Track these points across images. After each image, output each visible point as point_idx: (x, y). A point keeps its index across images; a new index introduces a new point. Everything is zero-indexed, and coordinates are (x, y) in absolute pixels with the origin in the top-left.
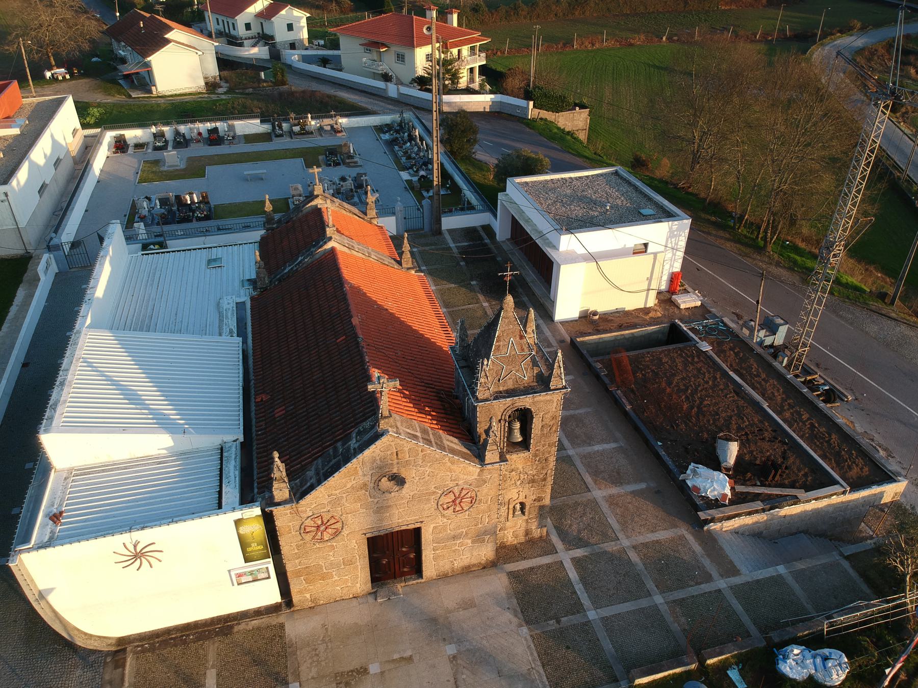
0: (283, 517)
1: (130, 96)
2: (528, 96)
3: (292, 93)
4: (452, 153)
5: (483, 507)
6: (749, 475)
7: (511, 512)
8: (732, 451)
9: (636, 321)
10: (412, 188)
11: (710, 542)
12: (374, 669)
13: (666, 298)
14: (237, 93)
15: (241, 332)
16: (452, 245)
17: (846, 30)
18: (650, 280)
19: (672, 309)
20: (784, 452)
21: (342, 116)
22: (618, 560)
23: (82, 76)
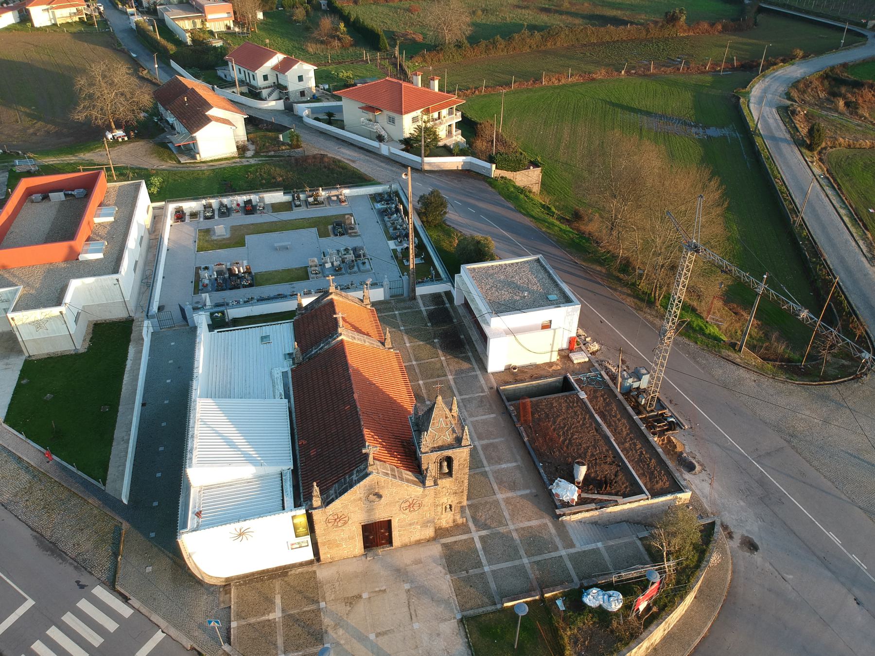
0: (317, 515)
1: (179, 162)
2: (491, 160)
3: (305, 158)
4: (426, 224)
5: (426, 508)
6: (591, 487)
8: (582, 472)
9: (543, 373)
10: (396, 257)
11: (561, 528)
12: (365, 596)
13: (565, 356)
14: (262, 156)
15: (287, 396)
16: (423, 309)
17: (788, 58)
18: (552, 345)
19: (569, 364)
20: (617, 472)
21: (345, 187)
22: (506, 538)
23: (139, 136)
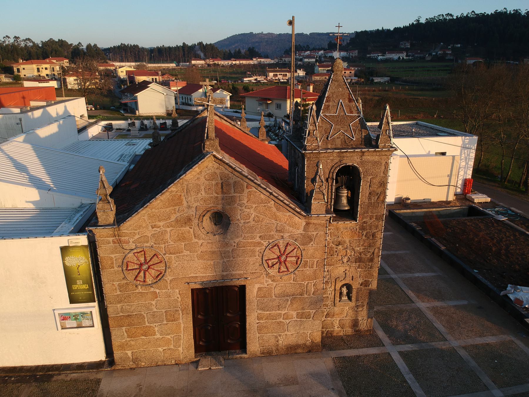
5: (308, 271)
7: (338, 295)
13: (462, 197)
18: (450, 176)
